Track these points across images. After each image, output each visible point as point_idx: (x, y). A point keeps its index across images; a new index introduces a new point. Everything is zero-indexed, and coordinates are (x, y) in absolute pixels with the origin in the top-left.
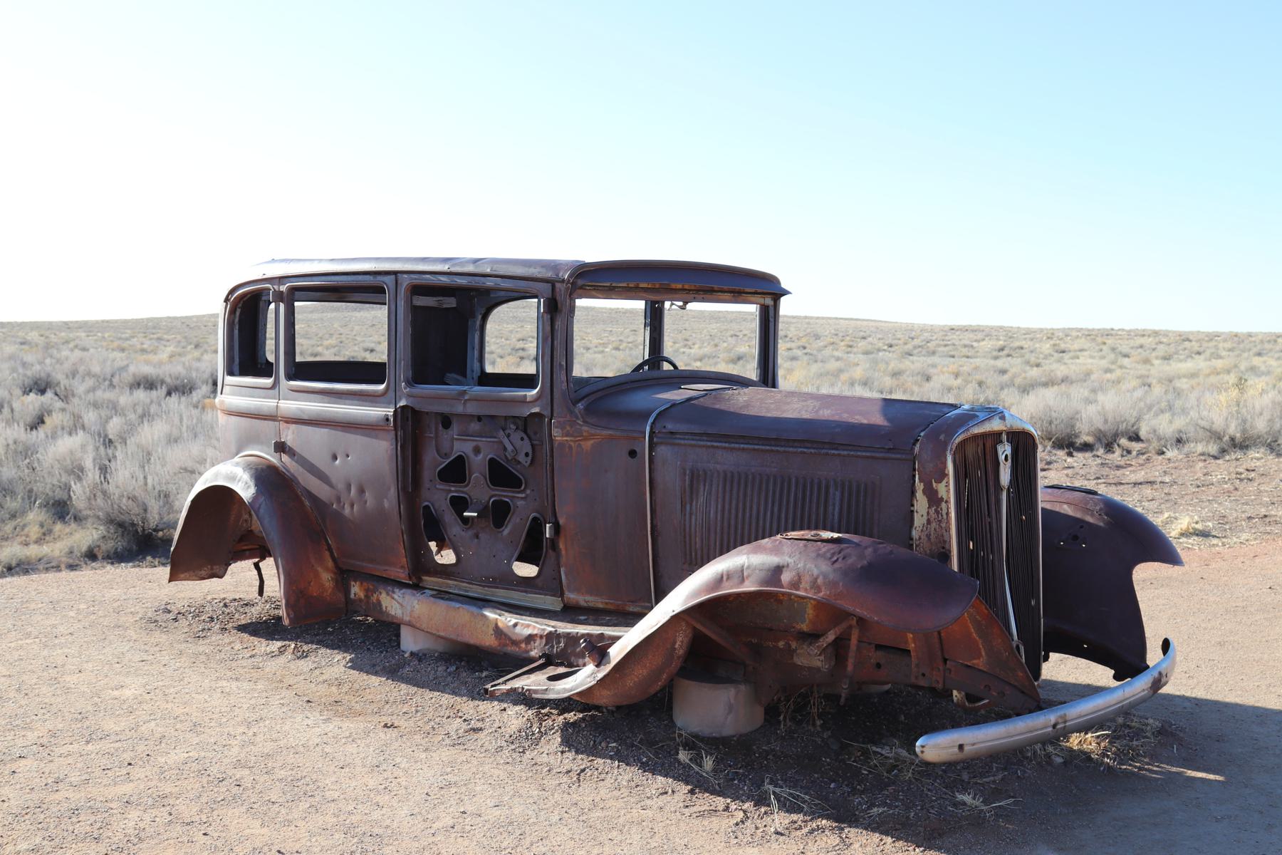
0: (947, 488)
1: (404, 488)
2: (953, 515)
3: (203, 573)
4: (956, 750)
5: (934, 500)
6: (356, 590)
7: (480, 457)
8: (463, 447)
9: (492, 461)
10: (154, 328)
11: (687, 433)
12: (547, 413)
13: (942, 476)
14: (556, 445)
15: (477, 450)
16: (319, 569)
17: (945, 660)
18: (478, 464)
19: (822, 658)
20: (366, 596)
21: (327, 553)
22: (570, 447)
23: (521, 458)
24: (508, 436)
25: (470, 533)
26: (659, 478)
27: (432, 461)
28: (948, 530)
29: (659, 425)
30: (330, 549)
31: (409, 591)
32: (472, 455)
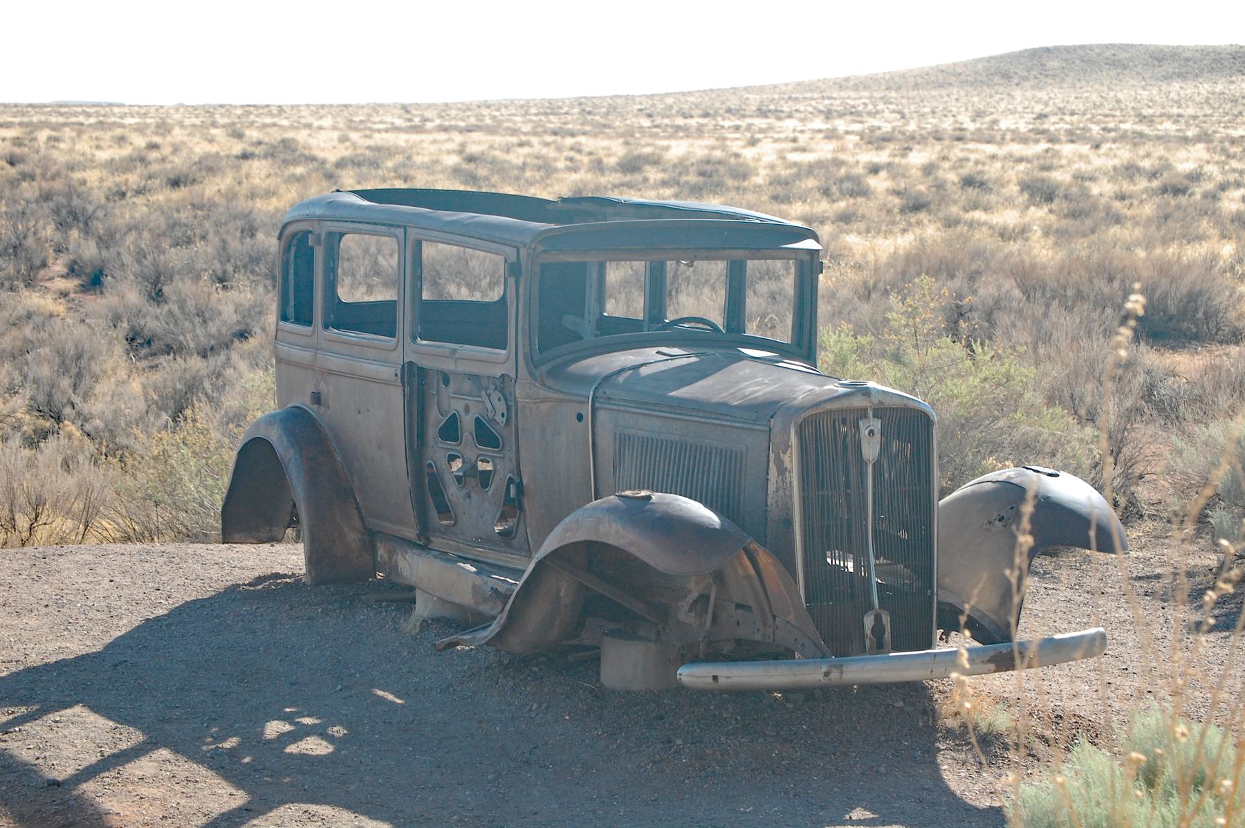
0: (792, 460)
1: (411, 445)
2: (795, 484)
3: (262, 535)
4: (711, 680)
5: (782, 470)
6: (382, 552)
7: (469, 417)
8: (457, 406)
9: (477, 419)
10: (762, 113)
11: (630, 401)
12: (513, 375)
13: (788, 447)
14: (520, 405)
15: (467, 409)
16: (346, 529)
17: (774, 617)
18: (468, 423)
19: (693, 614)
20: (390, 558)
21: (355, 511)
22: (531, 410)
23: (499, 419)
24: (489, 396)
25: (464, 492)
26: (599, 441)
27: (435, 419)
28: (791, 497)
29: (601, 391)
30: (358, 509)
31: (418, 552)
32: (463, 414)
